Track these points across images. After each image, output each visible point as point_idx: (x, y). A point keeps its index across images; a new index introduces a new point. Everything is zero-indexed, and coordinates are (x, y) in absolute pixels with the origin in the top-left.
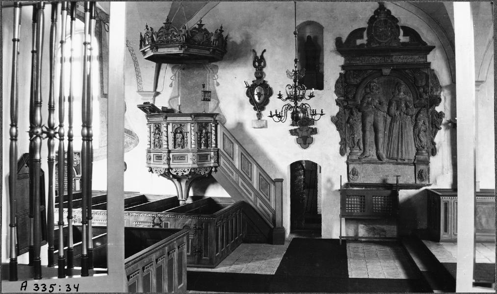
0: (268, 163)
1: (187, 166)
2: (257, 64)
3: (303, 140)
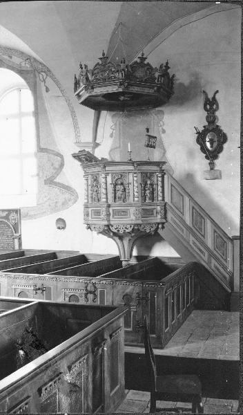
0: (223, 218)
1: (130, 222)
2: (208, 107)
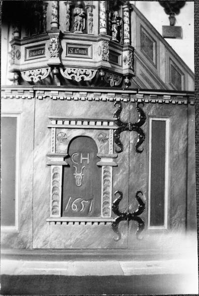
1: (92, 65)
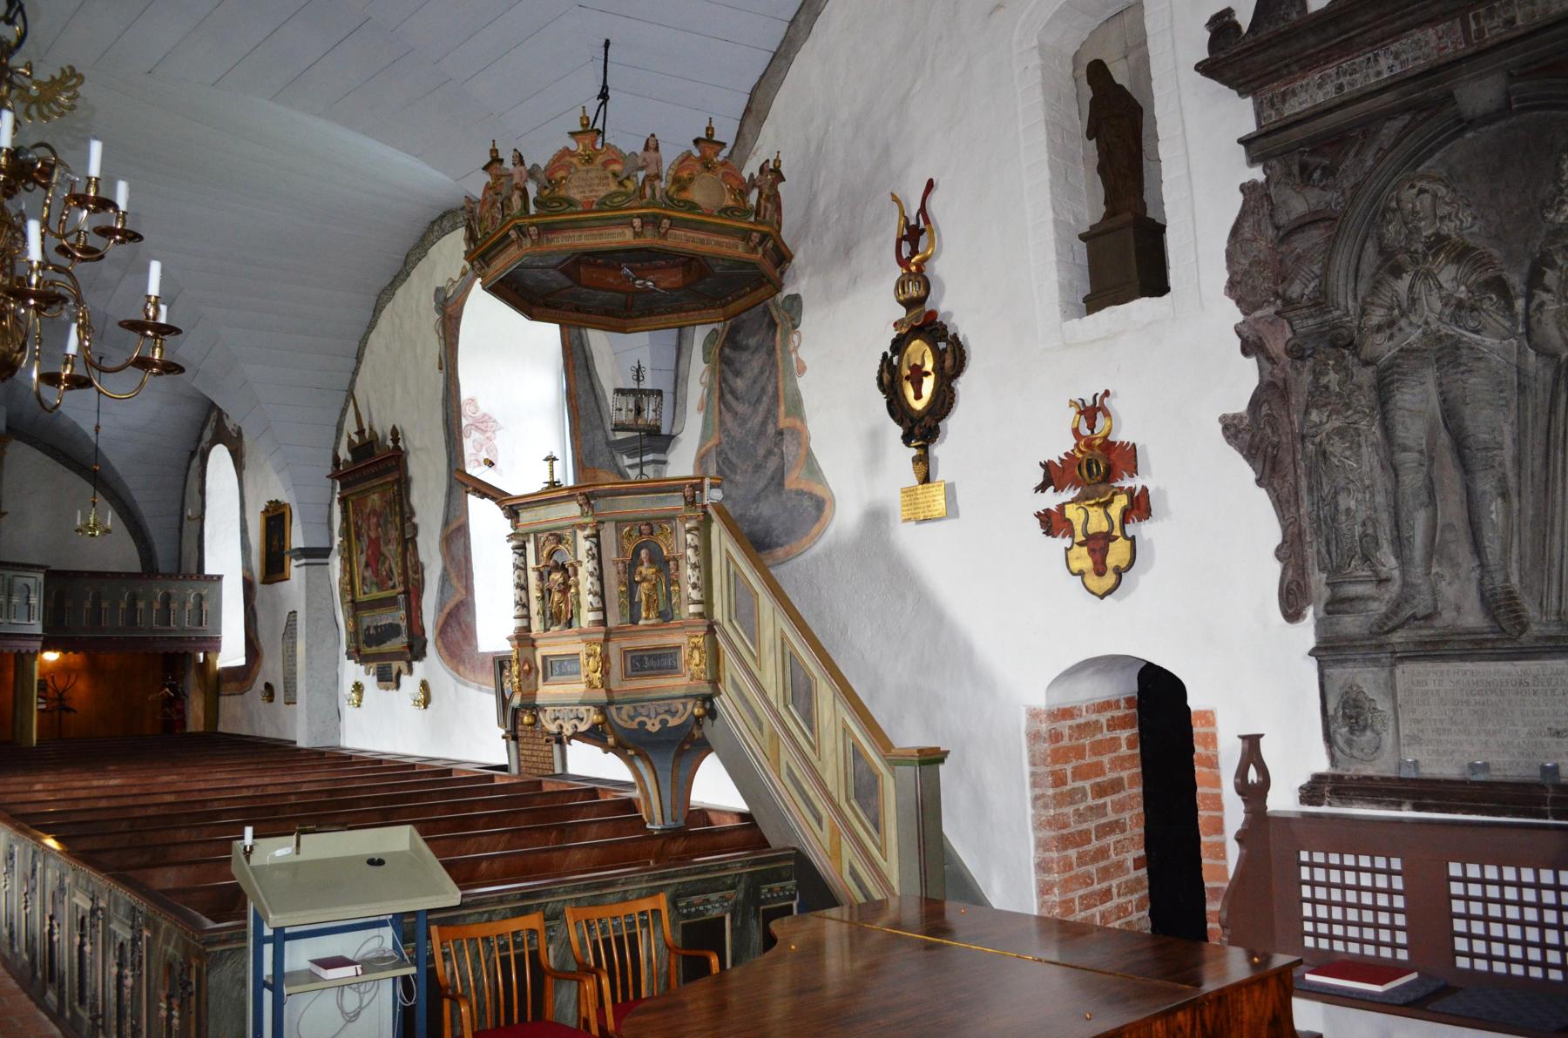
3: (1092, 552)
